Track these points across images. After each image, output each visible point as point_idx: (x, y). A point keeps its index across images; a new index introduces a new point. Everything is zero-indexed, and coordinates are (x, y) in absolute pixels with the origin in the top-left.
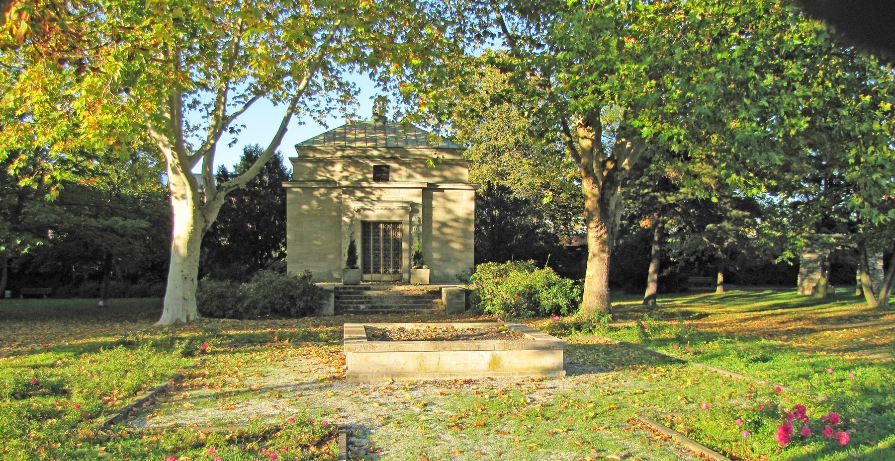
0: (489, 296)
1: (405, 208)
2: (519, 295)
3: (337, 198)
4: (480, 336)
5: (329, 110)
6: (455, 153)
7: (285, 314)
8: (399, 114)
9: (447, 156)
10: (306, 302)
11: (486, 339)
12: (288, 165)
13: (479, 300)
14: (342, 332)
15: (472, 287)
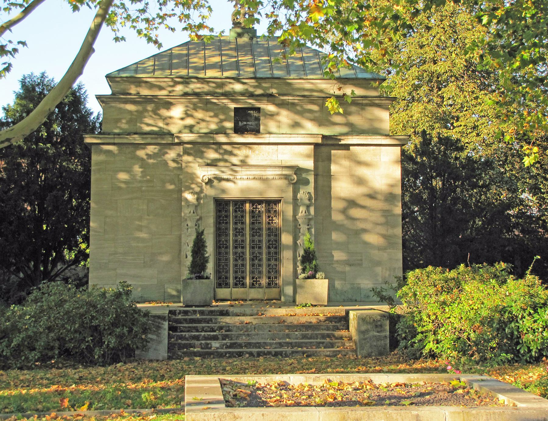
0: (430, 326)
1: (286, 177)
2: (482, 323)
3: (174, 161)
4: (421, 399)
5: (163, 18)
6: (368, 86)
7: (84, 358)
8: (276, 24)
9: (359, 92)
10: (120, 337)
11: (429, 403)
12: (94, 107)
13: (414, 334)
14: (181, 389)
15: (401, 309)
